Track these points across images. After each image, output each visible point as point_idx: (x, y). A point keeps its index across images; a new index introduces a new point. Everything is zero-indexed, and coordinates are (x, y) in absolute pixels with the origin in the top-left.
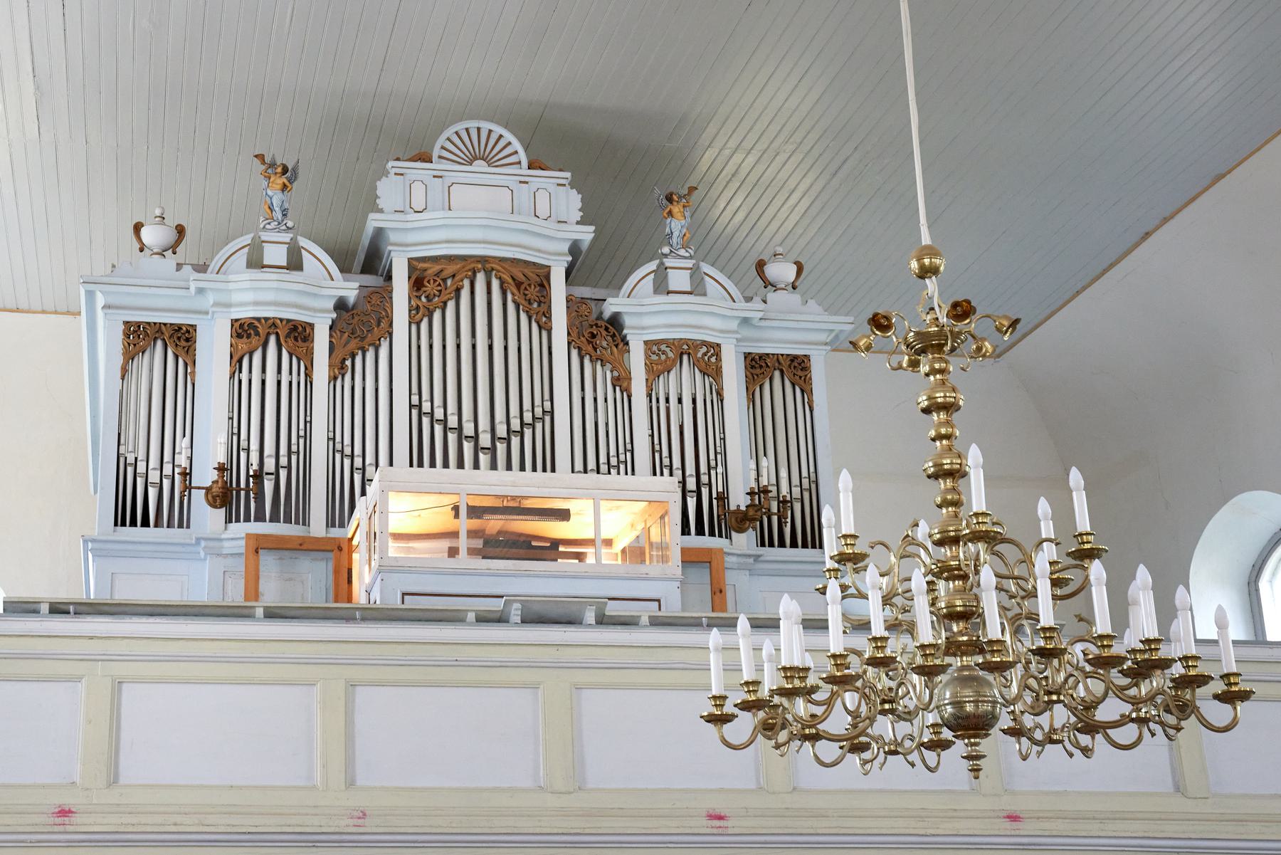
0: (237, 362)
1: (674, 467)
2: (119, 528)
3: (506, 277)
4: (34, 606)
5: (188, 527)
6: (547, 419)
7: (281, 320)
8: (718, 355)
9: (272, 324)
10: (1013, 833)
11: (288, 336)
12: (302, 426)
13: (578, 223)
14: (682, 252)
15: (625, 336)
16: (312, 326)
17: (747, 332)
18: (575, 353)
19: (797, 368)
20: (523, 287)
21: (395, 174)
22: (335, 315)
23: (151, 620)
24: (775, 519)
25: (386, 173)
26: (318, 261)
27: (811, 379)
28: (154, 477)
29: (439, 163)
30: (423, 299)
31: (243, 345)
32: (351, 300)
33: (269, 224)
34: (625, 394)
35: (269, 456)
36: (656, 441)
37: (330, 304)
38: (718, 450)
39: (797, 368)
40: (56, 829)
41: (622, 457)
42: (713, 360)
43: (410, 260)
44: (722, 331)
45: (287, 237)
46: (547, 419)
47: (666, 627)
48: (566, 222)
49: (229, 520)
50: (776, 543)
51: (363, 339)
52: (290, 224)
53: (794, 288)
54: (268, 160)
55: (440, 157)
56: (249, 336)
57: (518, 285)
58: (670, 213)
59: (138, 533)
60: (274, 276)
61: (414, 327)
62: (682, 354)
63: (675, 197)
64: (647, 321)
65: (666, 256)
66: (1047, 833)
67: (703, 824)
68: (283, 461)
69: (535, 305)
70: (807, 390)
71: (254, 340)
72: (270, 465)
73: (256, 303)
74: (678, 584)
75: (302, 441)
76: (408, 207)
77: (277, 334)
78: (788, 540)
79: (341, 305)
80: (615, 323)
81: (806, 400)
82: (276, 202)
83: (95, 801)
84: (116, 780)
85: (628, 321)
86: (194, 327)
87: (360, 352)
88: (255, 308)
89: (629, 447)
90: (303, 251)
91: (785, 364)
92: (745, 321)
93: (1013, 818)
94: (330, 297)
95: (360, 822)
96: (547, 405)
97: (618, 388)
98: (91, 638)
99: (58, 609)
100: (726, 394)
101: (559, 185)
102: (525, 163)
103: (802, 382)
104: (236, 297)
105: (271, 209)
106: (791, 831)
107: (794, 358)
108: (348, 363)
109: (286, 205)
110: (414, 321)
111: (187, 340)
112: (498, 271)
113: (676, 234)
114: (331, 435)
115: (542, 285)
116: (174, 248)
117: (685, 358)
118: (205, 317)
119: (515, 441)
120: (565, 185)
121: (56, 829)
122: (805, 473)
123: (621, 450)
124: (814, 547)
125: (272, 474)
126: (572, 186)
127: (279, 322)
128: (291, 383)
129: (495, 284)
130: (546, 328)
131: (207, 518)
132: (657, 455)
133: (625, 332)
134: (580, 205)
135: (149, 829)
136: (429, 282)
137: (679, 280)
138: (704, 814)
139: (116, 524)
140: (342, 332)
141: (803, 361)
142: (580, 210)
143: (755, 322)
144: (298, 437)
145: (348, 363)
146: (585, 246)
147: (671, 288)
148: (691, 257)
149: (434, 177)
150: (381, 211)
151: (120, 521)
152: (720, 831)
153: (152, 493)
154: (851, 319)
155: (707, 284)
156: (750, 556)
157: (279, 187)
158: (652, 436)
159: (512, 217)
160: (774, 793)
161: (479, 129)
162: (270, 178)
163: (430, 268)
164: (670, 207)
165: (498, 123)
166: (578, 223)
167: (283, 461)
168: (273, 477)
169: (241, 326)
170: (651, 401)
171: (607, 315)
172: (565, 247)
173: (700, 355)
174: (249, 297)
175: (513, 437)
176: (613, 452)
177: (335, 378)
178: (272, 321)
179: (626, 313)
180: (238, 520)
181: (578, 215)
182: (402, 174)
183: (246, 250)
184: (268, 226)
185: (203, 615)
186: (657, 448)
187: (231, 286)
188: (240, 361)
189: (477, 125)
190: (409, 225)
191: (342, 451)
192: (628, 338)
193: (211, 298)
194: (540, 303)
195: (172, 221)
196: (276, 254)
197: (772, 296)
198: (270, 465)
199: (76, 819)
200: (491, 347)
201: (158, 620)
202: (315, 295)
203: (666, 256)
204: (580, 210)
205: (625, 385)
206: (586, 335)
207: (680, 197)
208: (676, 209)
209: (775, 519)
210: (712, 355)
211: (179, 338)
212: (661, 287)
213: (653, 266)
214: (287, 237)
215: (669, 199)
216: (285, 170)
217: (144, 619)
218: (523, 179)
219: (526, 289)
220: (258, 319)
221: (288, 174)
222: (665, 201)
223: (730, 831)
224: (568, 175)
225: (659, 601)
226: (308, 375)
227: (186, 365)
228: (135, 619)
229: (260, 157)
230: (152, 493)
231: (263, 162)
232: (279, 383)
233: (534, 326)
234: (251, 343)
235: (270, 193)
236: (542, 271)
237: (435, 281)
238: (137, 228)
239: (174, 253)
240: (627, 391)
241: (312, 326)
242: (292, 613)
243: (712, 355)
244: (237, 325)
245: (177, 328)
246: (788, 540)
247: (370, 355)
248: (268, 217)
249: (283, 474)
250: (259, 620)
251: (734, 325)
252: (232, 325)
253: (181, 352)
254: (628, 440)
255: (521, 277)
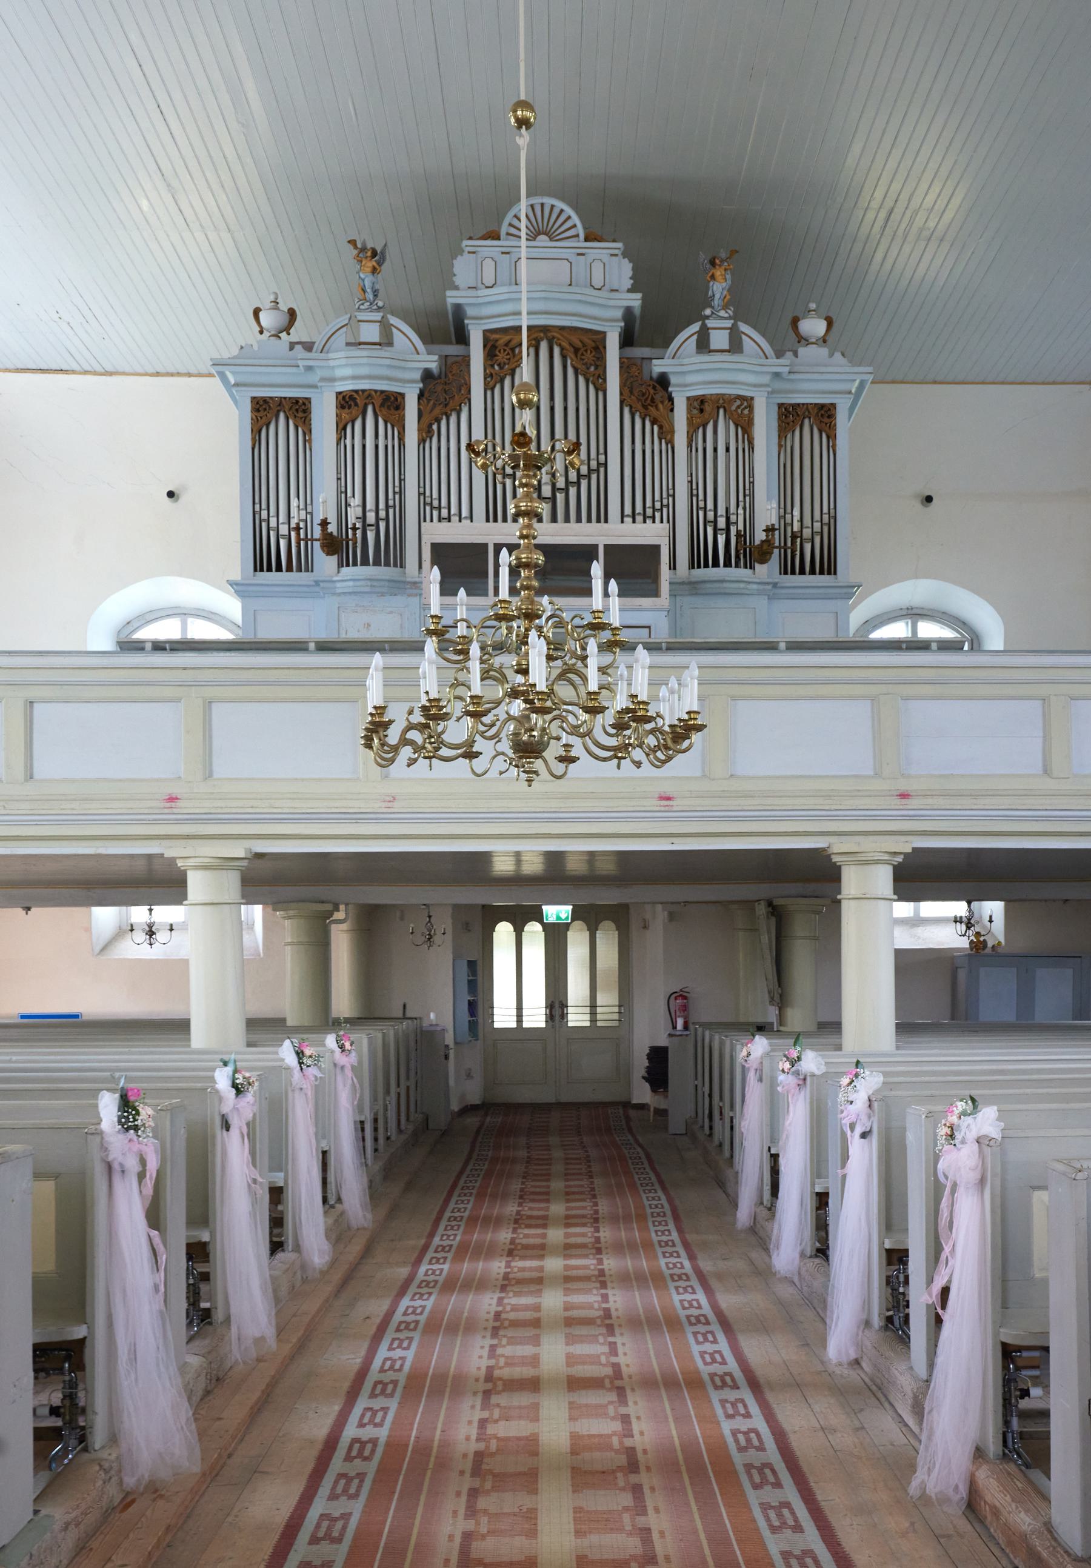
0: (341, 430)
1: (708, 508)
2: (258, 574)
3: (565, 344)
4: (141, 645)
5: (312, 571)
6: (602, 470)
7: (376, 391)
8: (751, 407)
9: (368, 396)
10: (901, 807)
11: (382, 405)
12: (397, 484)
13: (629, 291)
14: (722, 313)
15: (671, 393)
16: (402, 395)
17: (778, 385)
18: (626, 410)
19: (824, 415)
20: (580, 353)
21: (469, 252)
22: (421, 385)
23: (228, 654)
24: (789, 551)
25: (461, 252)
26: (406, 337)
27: (835, 425)
28: (283, 529)
29: (507, 240)
30: (496, 367)
31: (345, 415)
32: (436, 371)
33: (363, 304)
34: (669, 446)
35: (370, 511)
36: (694, 487)
37: (417, 375)
38: (747, 492)
39: (824, 415)
40: (166, 811)
41: (665, 502)
42: (746, 412)
43: (485, 332)
44: (755, 386)
45: (377, 316)
46: (602, 470)
47: (741, 651)
48: (617, 290)
49: (340, 565)
50: (797, 571)
51: (446, 405)
52: (380, 304)
53: (825, 341)
54: (359, 245)
55: (508, 234)
56: (350, 407)
57: (576, 351)
58: (713, 277)
59: (273, 577)
60: (365, 353)
61: (489, 393)
62: (718, 408)
63: (717, 261)
64: (690, 379)
65: (708, 317)
66: (928, 807)
67: (653, 804)
68: (382, 514)
69: (592, 369)
70: (832, 437)
71: (354, 410)
72: (371, 517)
73: (354, 378)
74: (666, 613)
75: (397, 497)
76: (480, 282)
77: (373, 403)
78: (808, 569)
79: (427, 375)
80: (663, 381)
81: (831, 444)
82: (368, 284)
83: (195, 791)
84: (211, 775)
85: (673, 380)
86: (309, 400)
87: (444, 417)
88: (354, 382)
89: (671, 492)
90: (393, 328)
91: (814, 412)
92: (777, 375)
93: (904, 796)
94: (418, 369)
95: (390, 804)
96: (602, 458)
97: (663, 441)
98: (185, 669)
99: (324, 647)
100: (756, 443)
101: (612, 255)
102: (582, 236)
103: (827, 428)
104: (339, 373)
105: (364, 291)
106: (723, 808)
107: (822, 406)
108: (435, 427)
109: (377, 287)
110: (488, 387)
111: (304, 411)
112: (559, 339)
113: (717, 296)
114: (422, 490)
115: (596, 348)
116: (287, 329)
117: (721, 411)
118: (316, 390)
119: (573, 491)
120: (616, 255)
121: (166, 811)
122: (825, 510)
123: (665, 495)
124: (829, 573)
125: (372, 525)
126: (625, 255)
127: (373, 393)
128: (386, 447)
129: (557, 351)
130: (601, 388)
131: (325, 563)
132: (694, 499)
133: (670, 389)
134: (630, 274)
135: (234, 811)
136: (500, 351)
137: (719, 339)
138: (657, 795)
139: (255, 570)
140: (429, 401)
141: (829, 409)
142: (631, 278)
143: (785, 376)
144: (394, 493)
145: (435, 427)
146: (637, 312)
147: (712, 347)
148: (730, 318)
149: (503, 253)
150: (457, 288)
151: (258, 567)
152: (667, 808)
153: (283, 543)
154: (870, 369)
155: (744, 343)
156: (768, 583)
157: (369, 270)
158: (691, 482)
159: (571, 289)
160: (714, 780)
161: (542, 205)
162: (361, 261)
163: (501, 339)
164: (713, 271)
165: (563, 199)
166: (629, 291)
167: (382, 514)
168: (373, 528)
169: (344, 398)
170: (691, 451)
171: (655, 375)
172: (619, 314)
173: (733, 408)
174: (348, 372)
175: (571, 488)
176: (657, 497)
177: (424, 441)
178: (366, 394)
179: (674, 373)
180: (348, 565)
181: (628, 283)
182: (474, 253)
183: (695, 337)
184: (362, 307)
185: (727, 649)
186: (695, 492)
187: (331, 363)
188: (345, 429)
189: (540, 201)
190: (480, 300)
191: (431, 504)
192: (674, 395)
193: (320, 373)
194: (597, 367)
195: (284, 307)
196: (371, 332)
197: (802, 351)
198: (371, 517)
199: (179, 804)
200: (566, 409)
201: (233, 654)
202: (404, 368)
203: (708, 317)
204: (631, 278)
205: (669, 437)
206: (636, 394)
207: (722, 261)
208: (718, 273)
209: (789, 551)
210: (746, 408)
211: (297, 410)
212: (703, 344)
213: (695, 327)
214: (729, 324)
215: (713, 263)
216: (374, 253)
217: (222, 654)
218: (504, 250)
219: (582, 354)
220: (356, 391)
221: (377, 258)
222: (708, 266)
223: (675, 809)
224: (620, 245)
225: (649, 627)
226: (401, 439)
227: (304, 434)
228: (215, 654)
229: (353, 242)
230: (283, 543)
231: (355, 247)
232: (377, 447)
233: (591, 387)
234: (351, 413)
235: (362, 276)
236: (598, 337)
237: (505, 350)
238: (256, 312)
239: (289, 334)
240: (671, 442)
241: (402, 395)
242: (338, 646)
243: (746, 408)
244: (340, 397)
245: (296, 401)
246: (808, 569)
247: (453, 419)
248: (361, 298)
249: (382, 525)
250: (311, 652)
251: (766, 379)
252: (337, 398)
253: (300, 423)
254: (670, 486)
255: (579, 344)
